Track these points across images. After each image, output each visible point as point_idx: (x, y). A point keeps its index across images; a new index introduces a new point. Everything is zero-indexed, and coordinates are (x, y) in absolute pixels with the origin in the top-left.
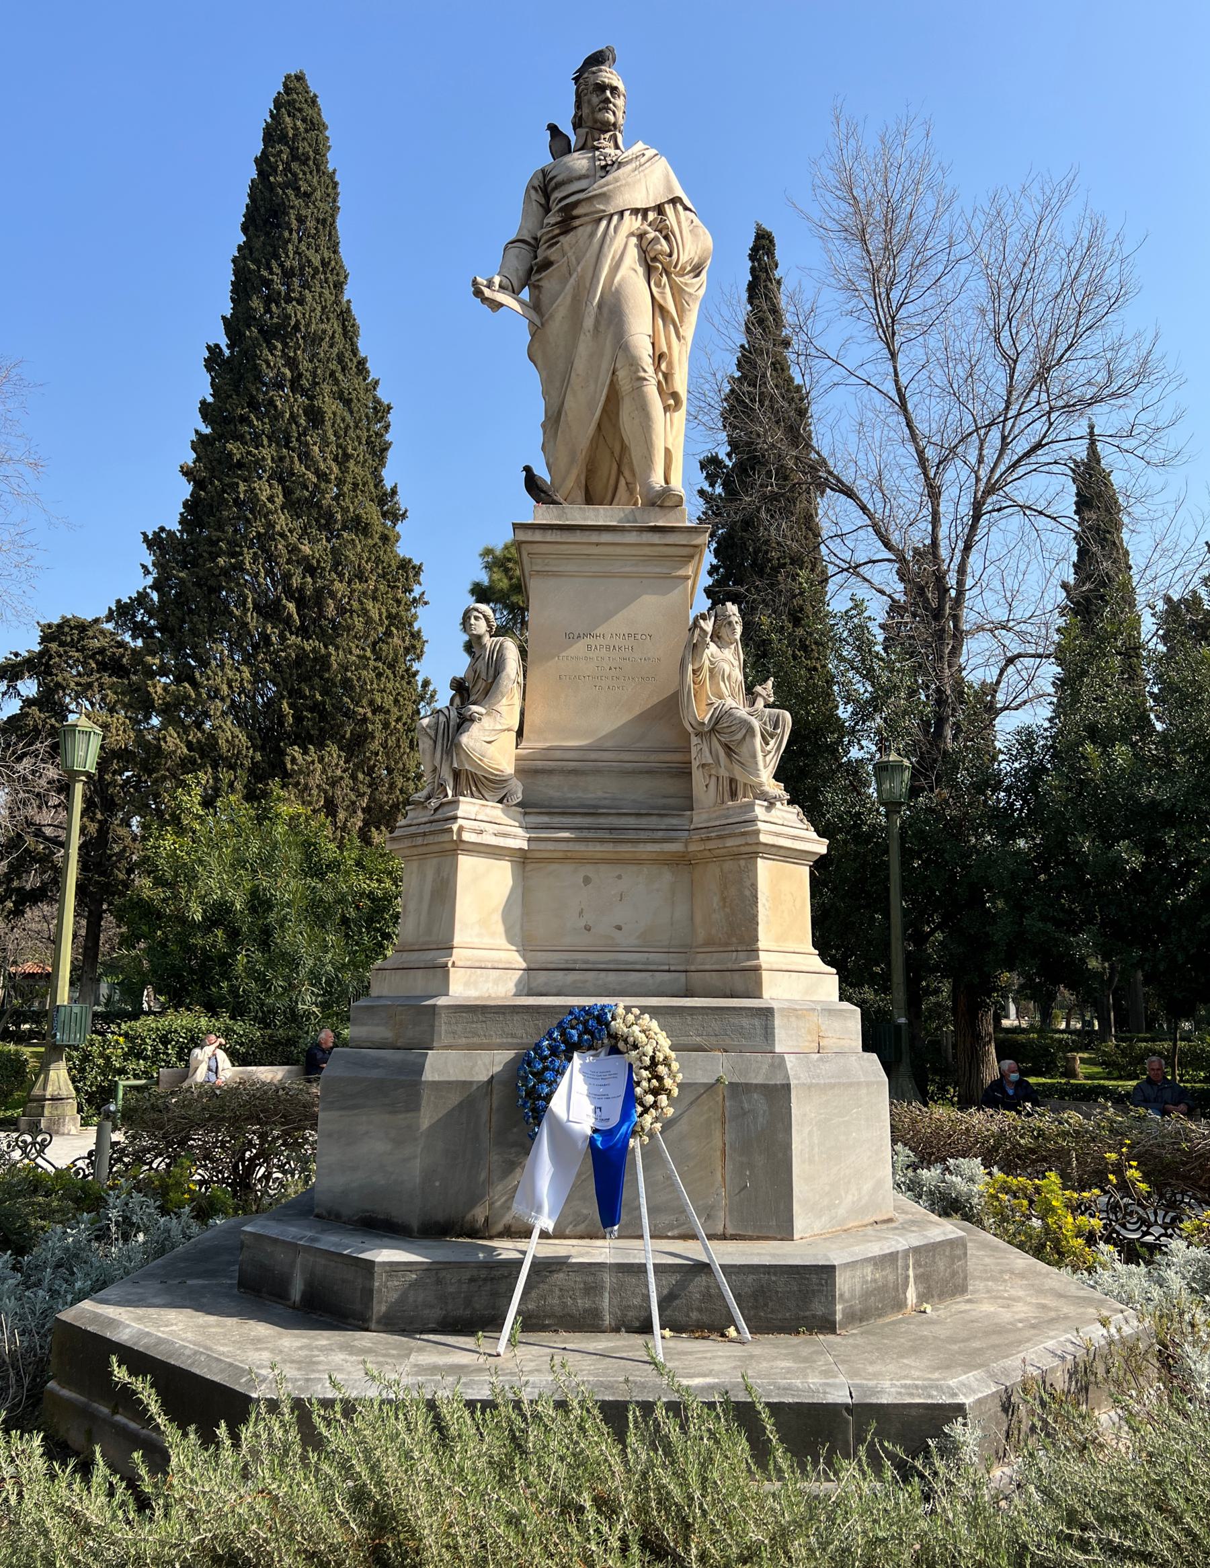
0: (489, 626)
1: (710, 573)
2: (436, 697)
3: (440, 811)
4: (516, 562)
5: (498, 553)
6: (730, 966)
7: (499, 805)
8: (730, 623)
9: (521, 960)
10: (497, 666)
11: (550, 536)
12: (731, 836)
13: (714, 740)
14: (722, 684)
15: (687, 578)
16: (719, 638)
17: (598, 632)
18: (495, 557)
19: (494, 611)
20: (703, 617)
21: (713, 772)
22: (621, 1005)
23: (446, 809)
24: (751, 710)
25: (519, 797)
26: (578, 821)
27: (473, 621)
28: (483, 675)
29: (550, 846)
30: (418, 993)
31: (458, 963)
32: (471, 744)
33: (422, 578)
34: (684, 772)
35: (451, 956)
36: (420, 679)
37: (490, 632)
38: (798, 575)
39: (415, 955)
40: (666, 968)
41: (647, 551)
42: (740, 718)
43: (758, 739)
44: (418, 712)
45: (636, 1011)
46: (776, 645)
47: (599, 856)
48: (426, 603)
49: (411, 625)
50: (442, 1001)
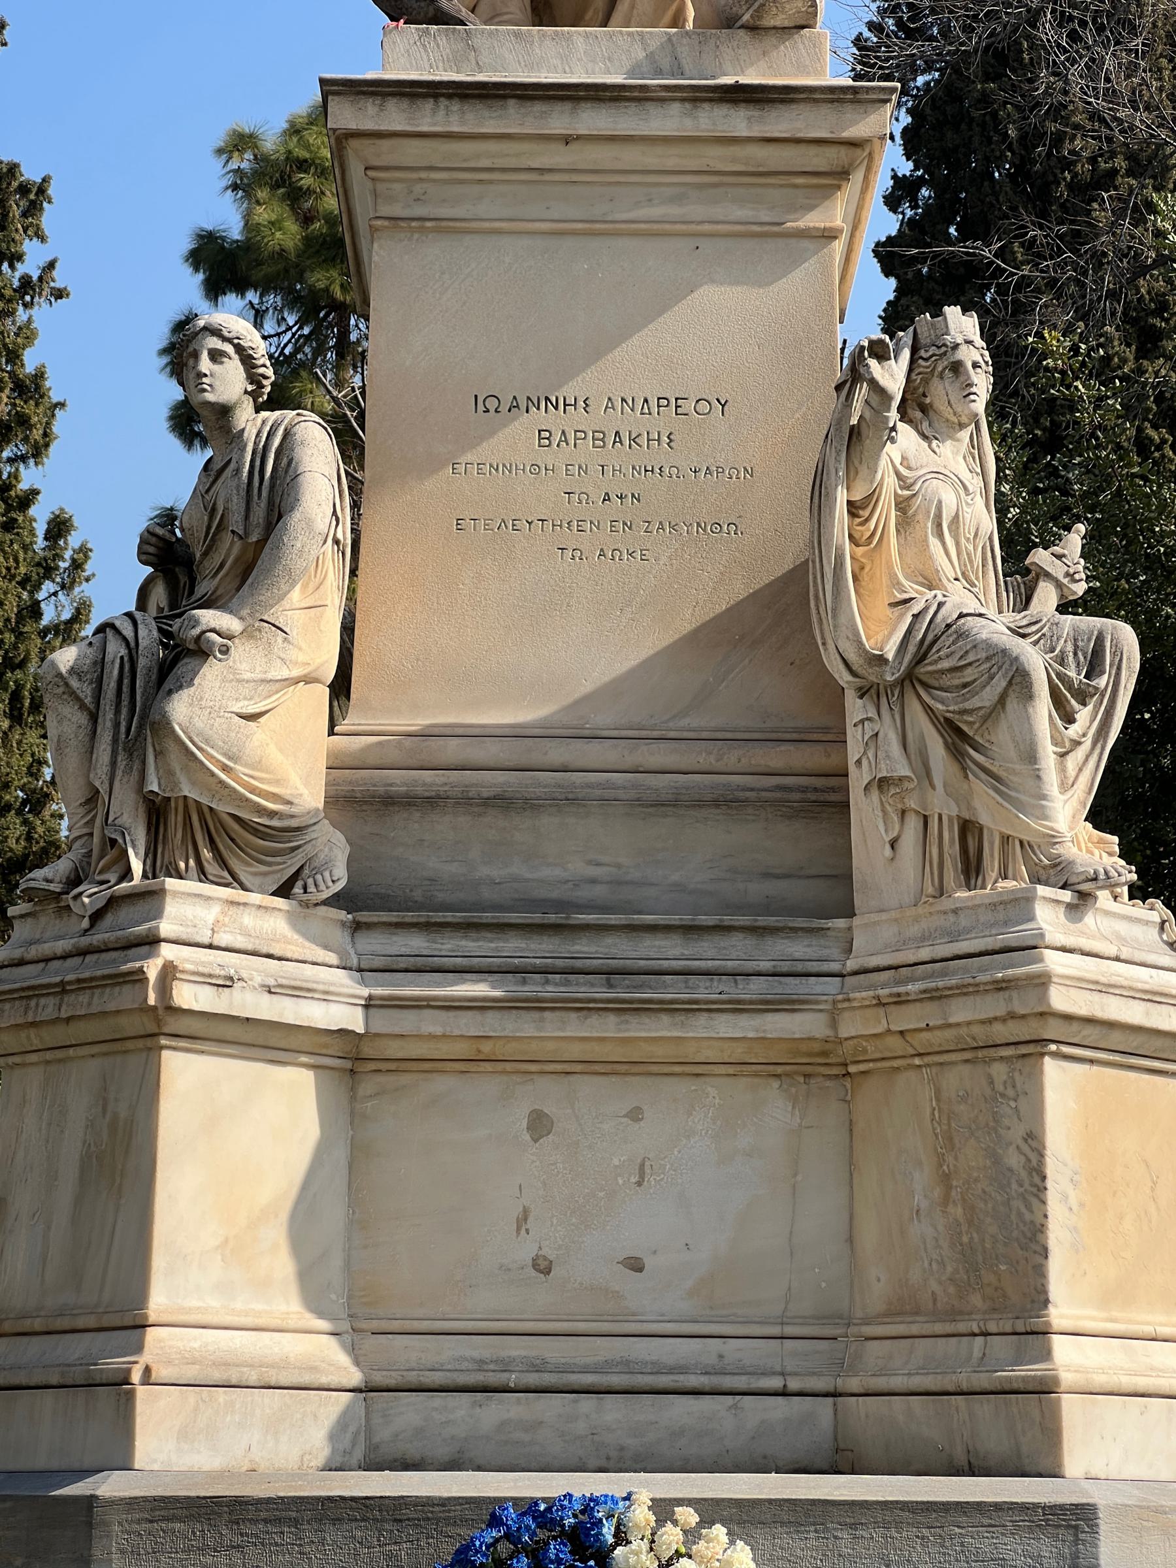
0: (254, 378)
1: (892, 202)
2: (89, 568)
3: (109, 920)
4: (322, 173)
5: (270, 142)
6: (965, 1379)
7: (280, 902)
8: (956, 367)
9: (343, 1359)
10: (275, 494)
11: (429, 118)
12: (964, 991)
13: (914, 708)
14: (934, 542)
15: (829, 235)
16: (924, 409)
17: (569, 391)
18: (261, 159)
19: (258, 320)
20: (879, 351)
21: (912, 803)
22: (644, 1497)
23: (124, 913)
24: (1021, 619)
25: (337, 877)
26: (513, 947)
27: (205, 364)
28: (236, 521)
29: (431, 1023)
30: (41, 1463)
31: (161, 1372)
32: (199, 723)
33: (48, 219)
34: (826, 803)
35: (139, 1348)
36: (40, 514)
37: (254, 395)
38: (1152, 208)
39: (33, 1348)
40: (775, 1383)
41: (715, 157)
42: (988, 644)
43: (1043, 706)
44: (35, 611)
45: (688, 1516)
46: (1087, 417)
47: (576, 1051)
48: (59, 294)
49: (14, 356)
50: (110, 1486)
